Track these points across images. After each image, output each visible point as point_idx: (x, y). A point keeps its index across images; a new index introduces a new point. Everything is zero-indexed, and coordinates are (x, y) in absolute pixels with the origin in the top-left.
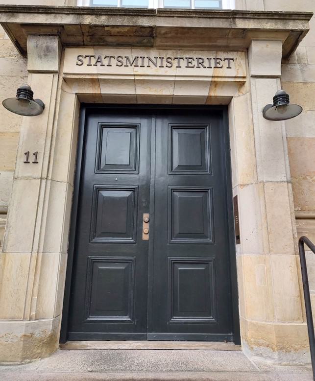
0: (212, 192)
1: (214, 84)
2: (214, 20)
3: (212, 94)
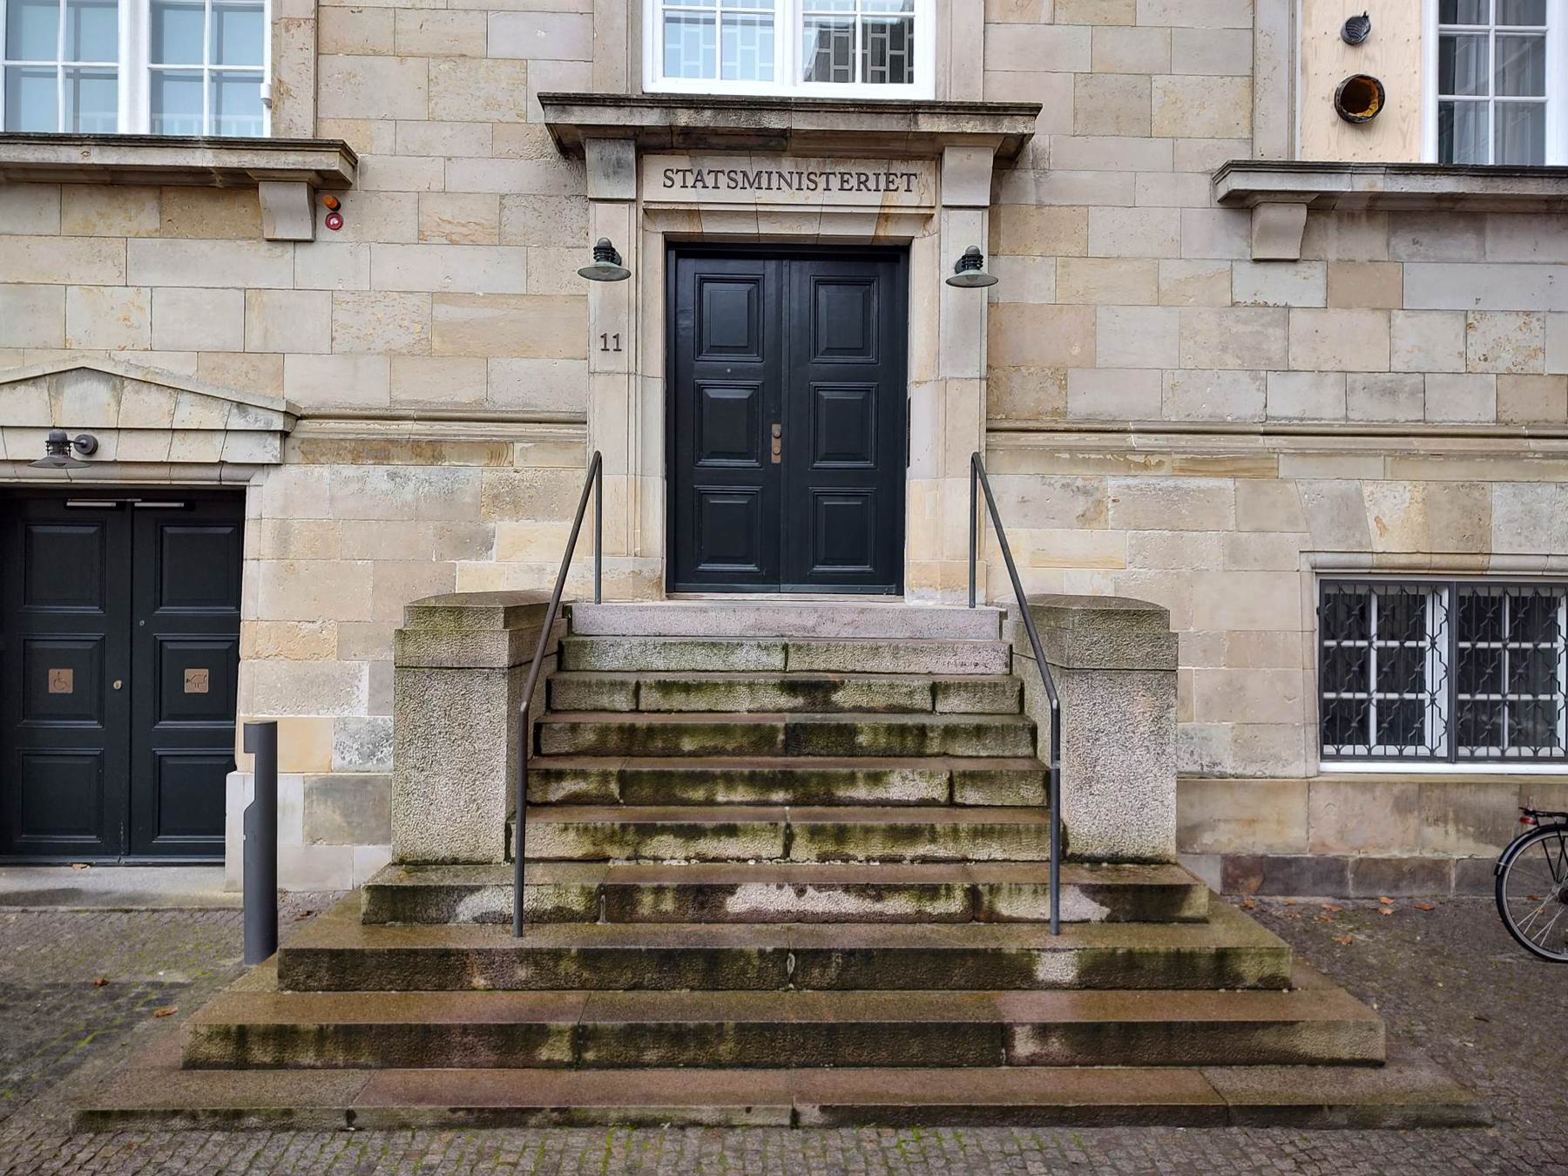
0: (877, 394)
1: (884, 218)
2: (885, 115)
3: (881, 233)
